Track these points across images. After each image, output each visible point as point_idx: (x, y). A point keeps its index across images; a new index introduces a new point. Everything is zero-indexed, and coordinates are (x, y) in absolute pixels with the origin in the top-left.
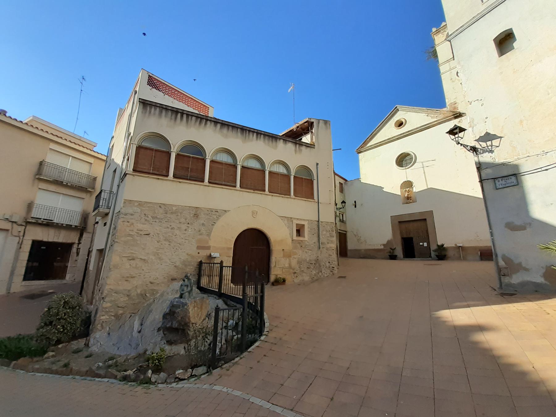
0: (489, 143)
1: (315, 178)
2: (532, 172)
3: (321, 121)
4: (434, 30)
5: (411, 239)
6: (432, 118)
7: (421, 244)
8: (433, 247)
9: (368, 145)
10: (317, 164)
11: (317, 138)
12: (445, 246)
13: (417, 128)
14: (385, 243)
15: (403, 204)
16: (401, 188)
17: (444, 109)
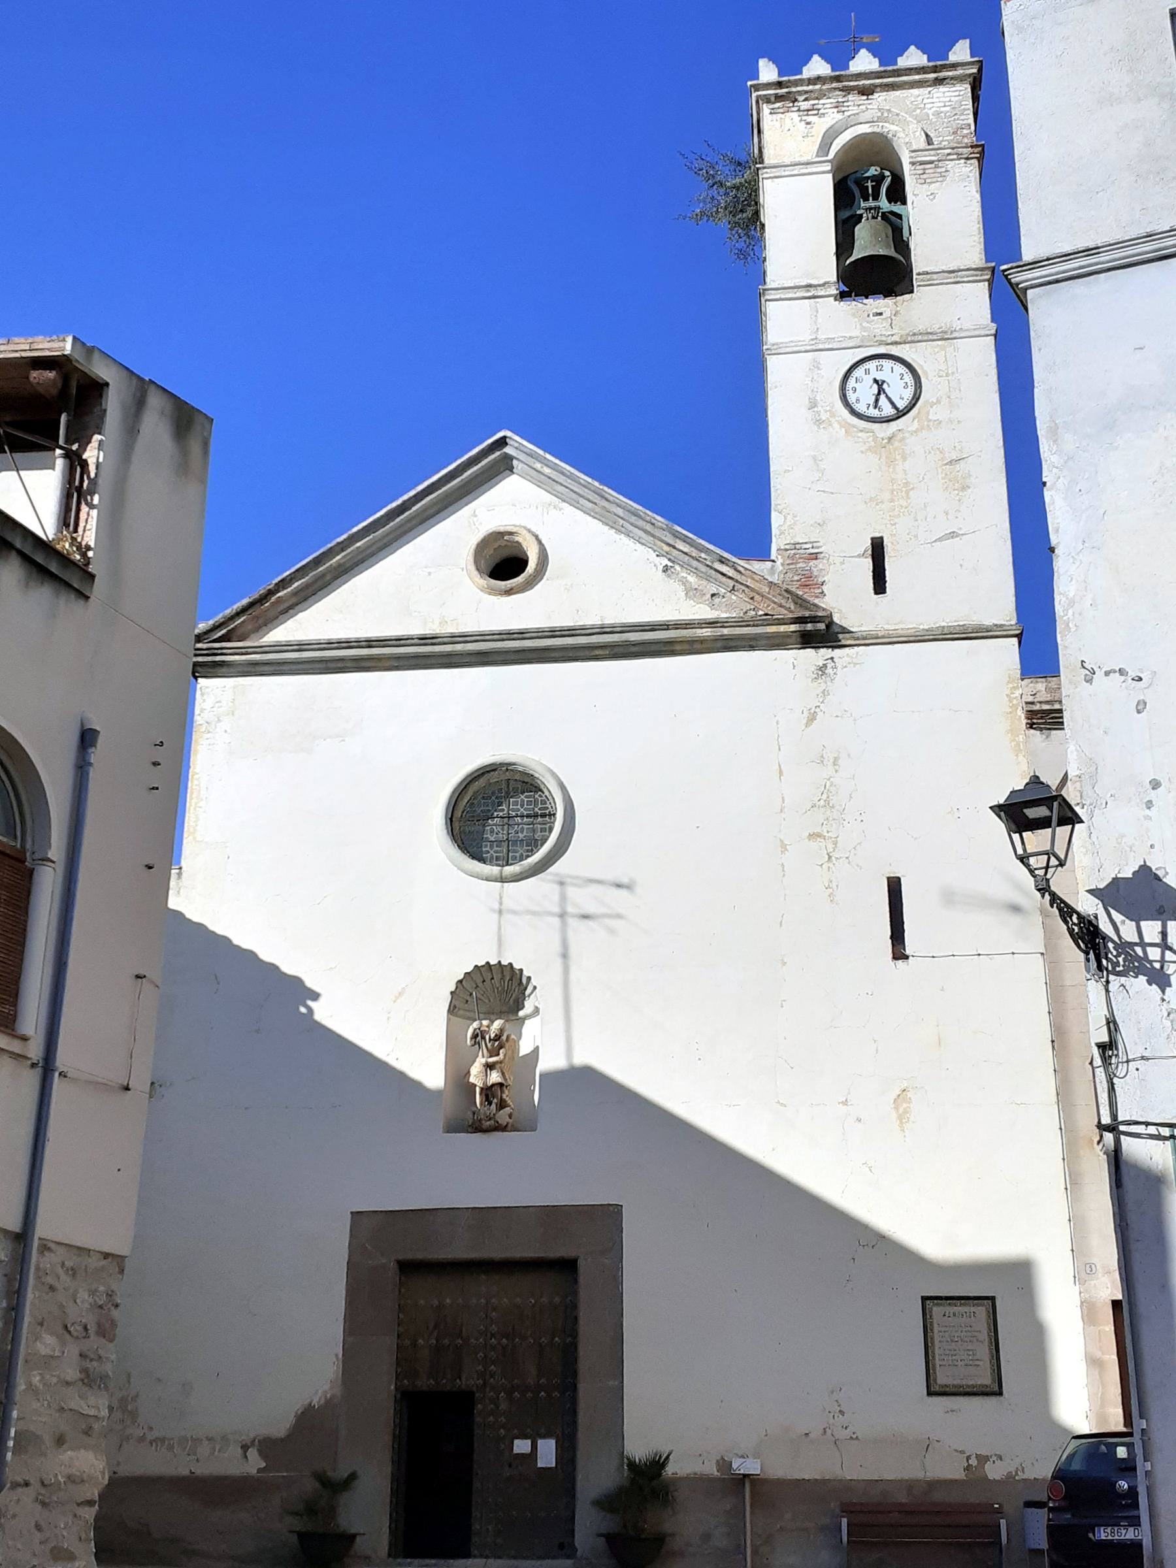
0: (1152, 930)
1: (57, 849)
3: (155, 401)
4: (768, 72)
5: (464, 1401)
6: (691, 593)
7: (522, 1446)
8: (597, 1477)
9: (281, 633)
10: (87, 738)
11: (112, 525)
12: (670, 1470)
13: (603, 630)
14: (279, 1424)
15: (454, 1127)
16: (452, 1010)
17: (757, 566)
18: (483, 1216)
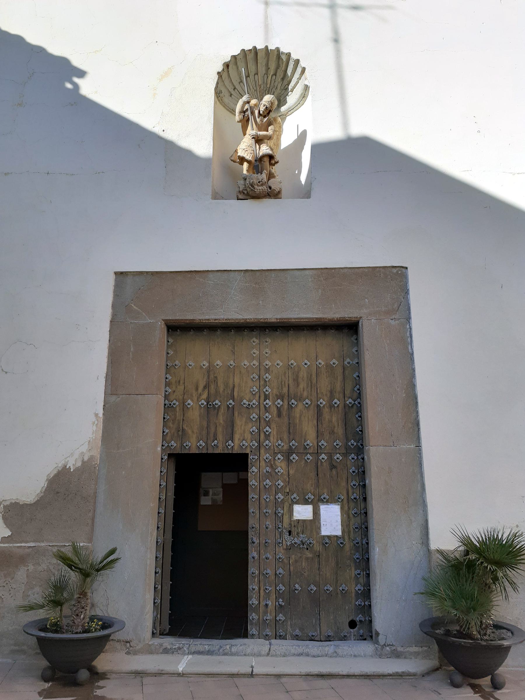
2: (345, 123)
7: (302, 512)
18: (258, 280)
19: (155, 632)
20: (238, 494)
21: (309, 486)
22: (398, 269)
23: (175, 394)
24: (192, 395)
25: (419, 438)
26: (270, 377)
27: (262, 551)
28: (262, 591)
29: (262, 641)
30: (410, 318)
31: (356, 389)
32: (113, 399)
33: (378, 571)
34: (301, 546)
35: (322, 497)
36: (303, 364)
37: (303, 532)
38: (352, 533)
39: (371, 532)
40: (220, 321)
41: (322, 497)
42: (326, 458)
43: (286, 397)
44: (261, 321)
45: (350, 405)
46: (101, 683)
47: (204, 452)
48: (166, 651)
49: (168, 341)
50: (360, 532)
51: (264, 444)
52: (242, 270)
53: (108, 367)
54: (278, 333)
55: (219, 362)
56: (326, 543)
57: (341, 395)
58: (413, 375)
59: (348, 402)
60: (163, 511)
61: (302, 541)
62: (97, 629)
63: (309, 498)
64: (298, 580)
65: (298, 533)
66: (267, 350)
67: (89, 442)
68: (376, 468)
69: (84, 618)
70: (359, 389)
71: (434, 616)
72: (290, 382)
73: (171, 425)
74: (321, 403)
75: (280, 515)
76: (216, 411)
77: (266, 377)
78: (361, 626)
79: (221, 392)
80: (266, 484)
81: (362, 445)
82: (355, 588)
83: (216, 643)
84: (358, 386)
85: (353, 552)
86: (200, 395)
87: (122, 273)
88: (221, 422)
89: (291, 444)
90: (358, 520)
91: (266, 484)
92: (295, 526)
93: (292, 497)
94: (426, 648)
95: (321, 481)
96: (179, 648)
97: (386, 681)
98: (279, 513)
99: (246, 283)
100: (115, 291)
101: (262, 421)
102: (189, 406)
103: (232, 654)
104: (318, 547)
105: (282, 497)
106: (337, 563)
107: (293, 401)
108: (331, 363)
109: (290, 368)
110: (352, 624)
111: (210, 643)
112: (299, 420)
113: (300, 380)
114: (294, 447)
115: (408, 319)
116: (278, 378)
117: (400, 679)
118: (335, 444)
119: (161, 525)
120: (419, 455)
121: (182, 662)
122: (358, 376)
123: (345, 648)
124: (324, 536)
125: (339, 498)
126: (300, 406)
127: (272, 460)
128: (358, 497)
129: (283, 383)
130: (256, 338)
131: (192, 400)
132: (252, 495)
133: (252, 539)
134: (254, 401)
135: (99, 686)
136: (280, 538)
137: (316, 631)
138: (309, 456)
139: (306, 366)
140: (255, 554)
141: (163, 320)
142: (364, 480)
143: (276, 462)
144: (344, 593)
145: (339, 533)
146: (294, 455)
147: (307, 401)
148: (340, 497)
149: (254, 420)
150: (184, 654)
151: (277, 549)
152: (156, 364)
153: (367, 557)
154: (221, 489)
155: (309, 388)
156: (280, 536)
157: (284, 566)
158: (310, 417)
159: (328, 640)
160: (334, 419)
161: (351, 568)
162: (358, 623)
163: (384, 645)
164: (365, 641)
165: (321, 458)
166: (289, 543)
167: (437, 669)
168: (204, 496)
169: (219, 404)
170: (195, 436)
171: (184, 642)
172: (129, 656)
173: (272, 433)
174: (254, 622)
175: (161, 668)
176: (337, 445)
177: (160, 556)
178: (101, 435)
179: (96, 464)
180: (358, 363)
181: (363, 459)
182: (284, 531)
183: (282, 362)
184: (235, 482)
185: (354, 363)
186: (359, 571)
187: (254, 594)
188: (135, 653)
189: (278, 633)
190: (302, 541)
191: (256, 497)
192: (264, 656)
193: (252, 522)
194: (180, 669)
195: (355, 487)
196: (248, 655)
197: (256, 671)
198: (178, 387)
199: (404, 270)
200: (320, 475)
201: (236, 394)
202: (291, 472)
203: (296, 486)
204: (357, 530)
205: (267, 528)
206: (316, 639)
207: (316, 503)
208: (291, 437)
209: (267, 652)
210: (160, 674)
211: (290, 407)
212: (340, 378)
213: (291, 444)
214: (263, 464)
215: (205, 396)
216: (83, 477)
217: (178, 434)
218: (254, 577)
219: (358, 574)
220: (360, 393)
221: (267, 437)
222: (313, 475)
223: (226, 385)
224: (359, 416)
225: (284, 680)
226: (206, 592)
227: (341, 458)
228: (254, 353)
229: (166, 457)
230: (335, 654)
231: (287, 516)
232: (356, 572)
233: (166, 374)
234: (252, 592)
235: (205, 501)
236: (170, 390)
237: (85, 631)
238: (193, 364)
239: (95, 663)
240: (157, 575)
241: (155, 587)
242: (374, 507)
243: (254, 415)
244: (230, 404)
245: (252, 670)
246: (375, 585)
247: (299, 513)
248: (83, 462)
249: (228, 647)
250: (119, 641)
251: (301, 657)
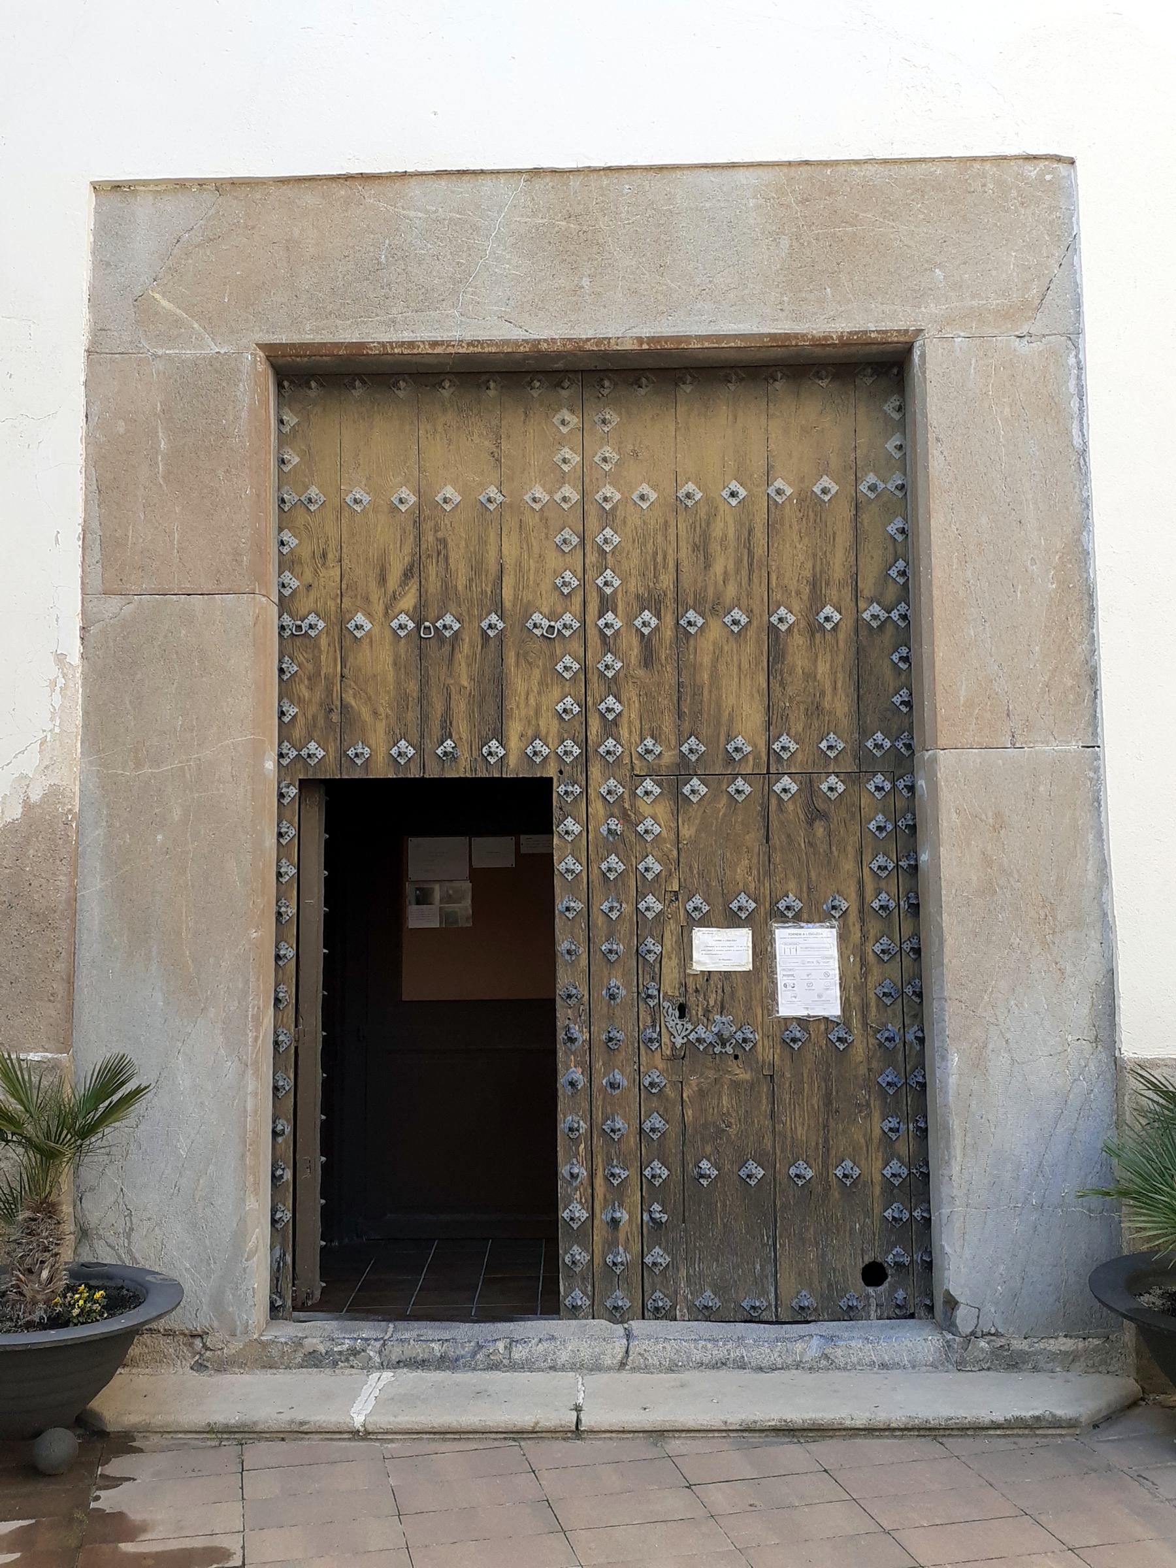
7: (720, 950)
18: (575, 202)
19: (279, 1303)
20: (522, 899)
21: (742, 871)
22: (1042, 164)
23: (313, 594)
24: (367, 599)
25: (1094, 722)
26: (616, 539)
27: (598, 1065)
28: (599, 1181)
29: (601, 1325)
30: (1079, 332)
31: (893, 573)
32: (113, 605)
33: (955, 1124)
34: (718, 1049)
35: (782, 905)
36: (725, 493)
37: (722, 1008)
38: (874, 1010)
39: (933, 1006)
40: (451, 350)
41: (782, 905)
42: (794, 788)
43: (670, 602)
44: (588, 347)
45: (875, 624)
46: (115, 1467)
47: (414, 773)
48: (314, 1360)
49: (281, 422)
50: (898, 1006)
51: (602, 750)
52: (519, 172)
53: (86, 502)
54: (642, 391)
55: (449, 491)
56: (794, 1040)
57: (847, 594)
58: (1084, 524)
59: (866, 616)
60: (291, 953)
61: (719, 1035)
62: (91, 1311)
63: (740, 908)
64: (708, 1149)
65: (707, 1012)
66: (608, 451)
67: (43, 742)
68: (954, 816)
69: (50, 1279)
70: (903, 573)
71: (1126, 1252)
72: (683, 554)
73: (306, 694)
74: (781, 620)
75: (651, 958)
76: (447, 648)
77: (606, 541)
78: (899, 1276)
79: (460, 588)
80: (610, 870)
81: (909, 747)
82: (880, 1170)
83: (465, 1334)
84: (901, 564)
85: (874, 1064)
86: (394, 597)
87: (117, 186)
88: (466, 684)
89: (685, 748)
90: (893, 971)
91: (610, 870)
92: (697, 991)
93: (690, 906)
94: (1096, 1342)
95: (777, 858)
96: (354, 1352)
97: (982, 1444)
98: (649, 952)
99: (534, 214)
100: (97, 250)
101: (594, 679)
102: (358, 634)
103: (514, 1367)
104: (768, 1052)
105: (658, 907)
106: (828, 1100)
107: (691, 615)
108: (817, 489)
109: (681, 508)
110: (874, 1274)
111: (447, 1336)
112: (711, 676)
113: (715, 547)
114: (693, 758)
115: (1074, 336)
116: (644, 544)
117: (1026, 1436)
118: (823, 745)
119: (287, 992)
120: (1091, 774)
121: (366, 1390)
122: (903, 531)
123: (853, 1344)
124: (786, 1019)
125: (834, 908)
126: (715, 631)
127: (626, 796)
128: (892, 904)
129: (659, 558)
130: (572, 411)
131: (369, 615)
132: (565, 902)
133: (567, 1029)
134: (567, 618)
135: (107, 1477)
136: (654, 1026)
137: (764, 1293)
138: (740, 782)
139: (734, 502)
140: (577, 1074)
141: (261, 346)
142: (912, 851)
143: (639, 803)
144: (852, 1188)
145: (834, 1010)
146: (695, 781)
147: (736, 614)
148: (836, 903)
149: (567, 675)
150: (368, 1367)
151: (643, 1059)
152: (245, 493)
153: (920, 1079)
154: (468, 885)
155: (744, 572)
156: (654, 1021)
157: (666, 1110)
158: (745, 665)
159: (799, 1318)
160: (823, 669)
161: (869, 1115)
162: (889, 1272)
163: (973, 1333)
164: (911, 1322)
165: (778, 788)
166: (679, 1041)
167: (1134, 1404)
168: (418, 903)
169: (456, 626)
170: (381, 726)
171: (367, 1332)
172: (203, 1378)
173: (625, 714)
174: (577, 1270)
175: (300, 1417)
176: (830, 747)
177: (287, 1084)
178: (79, 722)
179: (70, 810)
180: (902, 487)
181: (911, 788)
182: (666, 1004)
183: (655, 487)
184: (509, 862)
185: (891, 486)
186: (894, 1123)
187: (576, 1189)
188: (222, 1366)
189: (650, 1304)
190: (719, 1035)
191: (579, 905)
192: (609, 1369)
193: (566, 980)
194: (358, 1421)
195: (884, 874)
196: (563, 1368)
197: (589, 1420)
198: (323, 573)
199: (1062, 169)
200: (775, 840)
201: (507, 594)
202: (687, 832)
203: (701, 874)
204: (888, 1001)
205: (612, 997)
206: (765, 1316)
207: (761, 923)
208: (686, 726)
209: (619, 1357)
210: (298, 1432)
211: (683, 635)
212: (844, 538)
213: (685, 748)
214: (597, 808)
215: (408, 601)
216: (31, 852)
217: (327, 719)
218: (576, 1142)
219: (891, 1129)
220: (905, 586)
221: (610, 727)
222: (753, 838)
223: (477, 567)
224: (901, 658)
225: (675, 1445)
226: (438, 1148)
227: (841, 788)
228: (564, 461)
229: (293, 791)
230: (824, 1362)
231: (674, 962)
232: (886, 1126)
233: (281, 530)
234: (570, 1183)
235: (420, 918)
236: (295, 583)
237: (58, 1321)
238: (366, 499)
239: (96, 1404)
240: (280, 1140)
241: (273, 1176)
242: (946, 935)
243: (568, 660)
244: (490, 626)
245: (578, 1421)
246: (948, 1163)
247: (708, 950)
248: (28, 806)
249: (501, 1346)
250: (169, 1333)
251: (722, 1373)
